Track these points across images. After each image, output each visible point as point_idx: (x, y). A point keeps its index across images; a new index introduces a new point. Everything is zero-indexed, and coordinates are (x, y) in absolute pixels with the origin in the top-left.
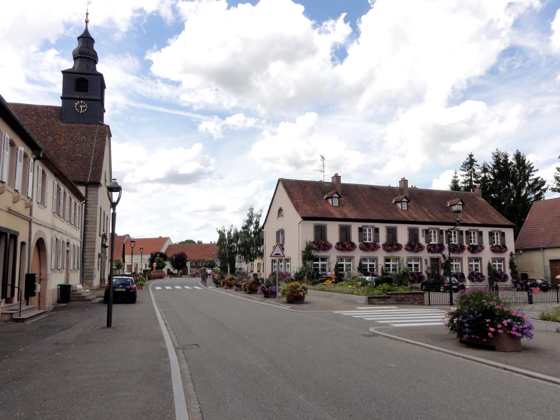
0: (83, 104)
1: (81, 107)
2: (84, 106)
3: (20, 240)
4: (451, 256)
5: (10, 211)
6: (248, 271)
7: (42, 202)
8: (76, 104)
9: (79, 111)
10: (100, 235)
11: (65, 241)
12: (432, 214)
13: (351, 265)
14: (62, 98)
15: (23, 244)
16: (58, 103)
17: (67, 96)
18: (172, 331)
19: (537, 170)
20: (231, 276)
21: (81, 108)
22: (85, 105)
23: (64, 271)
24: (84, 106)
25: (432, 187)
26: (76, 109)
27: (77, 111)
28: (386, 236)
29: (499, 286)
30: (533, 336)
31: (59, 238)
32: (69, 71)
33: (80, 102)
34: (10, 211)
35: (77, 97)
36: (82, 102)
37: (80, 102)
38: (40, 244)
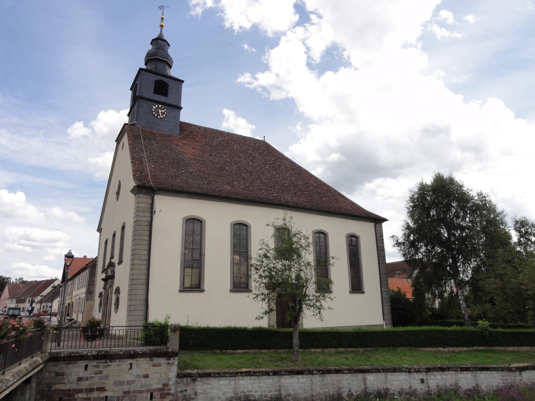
0: (161, 109)
1: (160, 111)
2: (163, 111)
6: (509, 227)
8: (154, 107)
9: (157, 116)
18: (182, 399)
19: (326, 301)
21: (160, 113)
22: (164, 110)
24: (163, 111)
25: (350, 193)
26: (154, 113)
27: (154, 115)
28: (359, 329)
29: (193, 283)
30: (294, 231)
33: (158, 106)
36: (160, 106)
37: (158, 106)
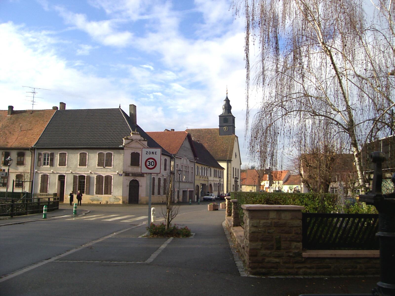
3: (206, 185)
4: (14, 191)
5: (204, 180)
7: (211, 176)
10: (233, 178)
11: (217, 183)
12: (168, 203)
13: (104, 198)
14: (219, 126)
15: (207, 186)
16: (218, 127)
17: (221, 125)
20: (75, 204)
23: (217, 191)
31: (215, 183)
32: (221, 116)
34: (204, 180)
35: (224, 125)
38: (211, 185)
